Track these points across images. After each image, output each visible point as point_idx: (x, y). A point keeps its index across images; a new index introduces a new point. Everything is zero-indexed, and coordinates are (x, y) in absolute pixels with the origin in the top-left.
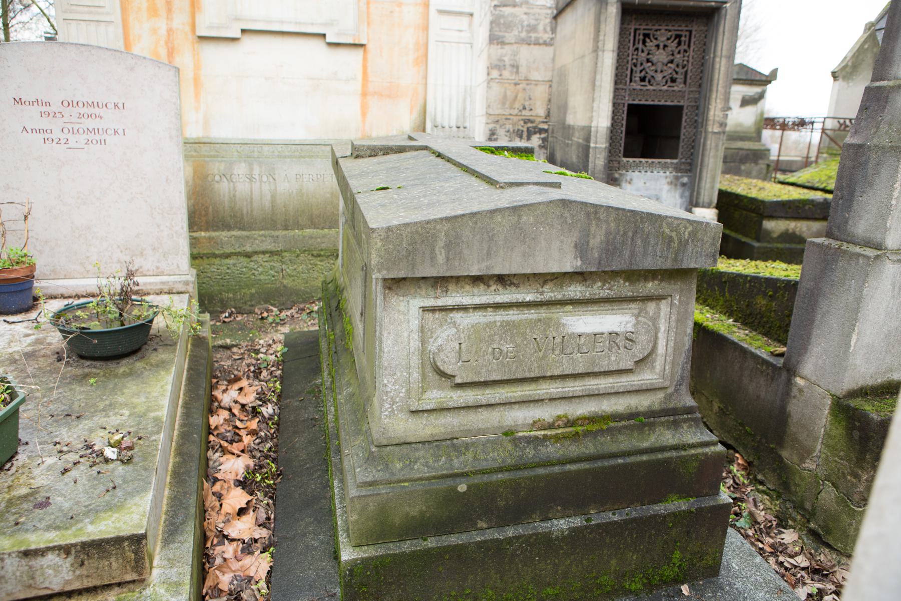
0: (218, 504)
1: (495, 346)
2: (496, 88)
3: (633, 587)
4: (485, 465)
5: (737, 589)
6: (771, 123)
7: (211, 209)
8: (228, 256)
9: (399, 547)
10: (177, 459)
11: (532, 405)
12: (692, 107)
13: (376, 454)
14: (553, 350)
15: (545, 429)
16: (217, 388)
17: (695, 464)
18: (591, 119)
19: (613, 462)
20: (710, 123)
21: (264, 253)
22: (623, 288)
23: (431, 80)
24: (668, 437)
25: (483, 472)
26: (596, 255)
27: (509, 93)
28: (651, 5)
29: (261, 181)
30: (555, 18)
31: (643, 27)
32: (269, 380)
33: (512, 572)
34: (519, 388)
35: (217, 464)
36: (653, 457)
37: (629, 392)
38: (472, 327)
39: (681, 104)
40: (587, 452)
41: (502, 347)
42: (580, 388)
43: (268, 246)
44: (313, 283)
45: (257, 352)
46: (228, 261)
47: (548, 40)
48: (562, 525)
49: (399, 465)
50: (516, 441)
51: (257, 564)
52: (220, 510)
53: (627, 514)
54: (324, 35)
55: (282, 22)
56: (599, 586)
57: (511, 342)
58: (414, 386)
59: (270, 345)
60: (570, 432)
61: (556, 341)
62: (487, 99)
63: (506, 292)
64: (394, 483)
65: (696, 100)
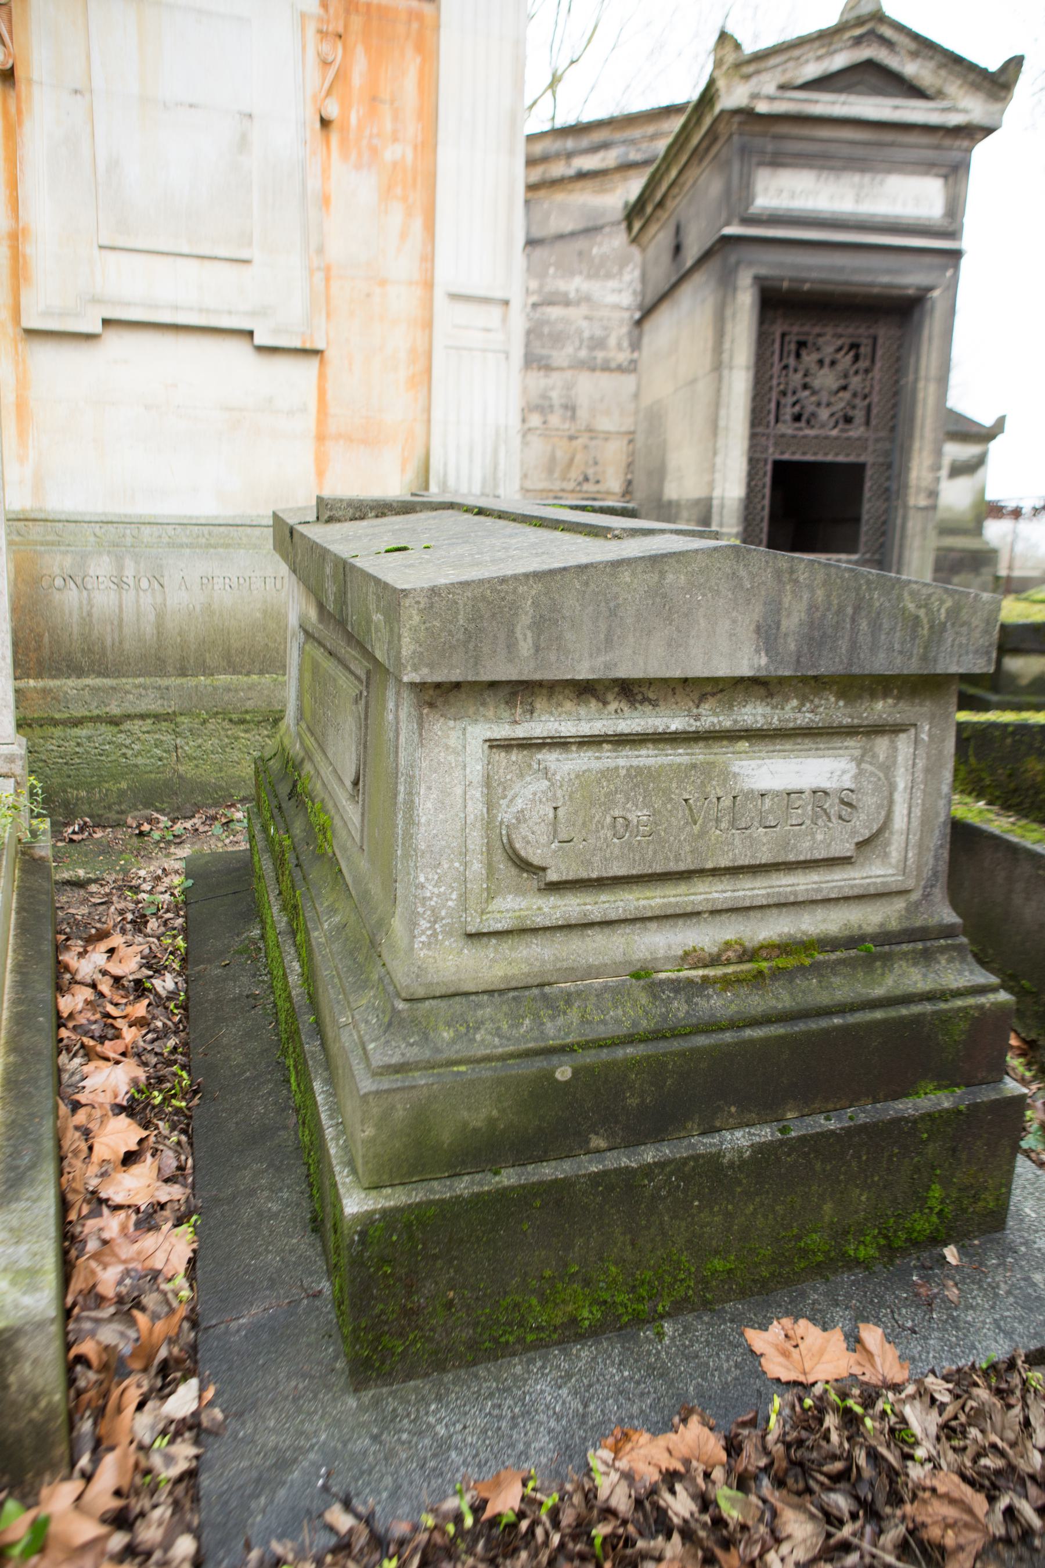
0: (84, 1146)
1: (617, 813)
2: (538, 446)
3: (862, 1253)
4: (602, 1031)
5: (1039, 1250)
6: (996, 510)
7: (46, 639)
8: (77, 722)
9: (451, 1188)
10: (11, 1059)
11: (680, 922)
12: (882, 465)
13: (405, 1015)
14: (718, 820)
15: (705, 966)
16: (67, 948)
17: (964, 1026)
18: (711, 484)
19: (824, 1023)
20: (912, 491)
21: (143, 717)
22: (833, 710)
23: (437, 414)
24: (915, 979)
25: (599, 1044)
26: (792, 647)
27: (559, 454)
28: (809, 293)
29: (138, 587)
30: (639, 323)
31: (796, 330)
32: (163, 934)
33: (652, 1230)
34: (658, 892)
35: (77, 1077)
36: (892, 1013)
37: (847, 899)
38: (577, 776)
39: (862, 459)
40: (780, 1006)
41: (629, 816)
42: (763, 892)
43: (150, 704)
44: (231, 771)
45: (136, 889)
46: (77, 731)
47: (625, 364)
48: (739, 1140)
49: (447, 1035)
50: (655, 989)
51: (166, 1246)
52: (89, 1156)
53: (851, 1118)
54: (251, 333)
55: (176, 308)
56: (804, 1253)
57: (646, 805)
58: (474, 887)
59: (158, 878)
60: (749, 971)
61: (722, 804)
62: (522, 463)
63: (636, 714)
64: (441, 1066)
65: (888, 453)
